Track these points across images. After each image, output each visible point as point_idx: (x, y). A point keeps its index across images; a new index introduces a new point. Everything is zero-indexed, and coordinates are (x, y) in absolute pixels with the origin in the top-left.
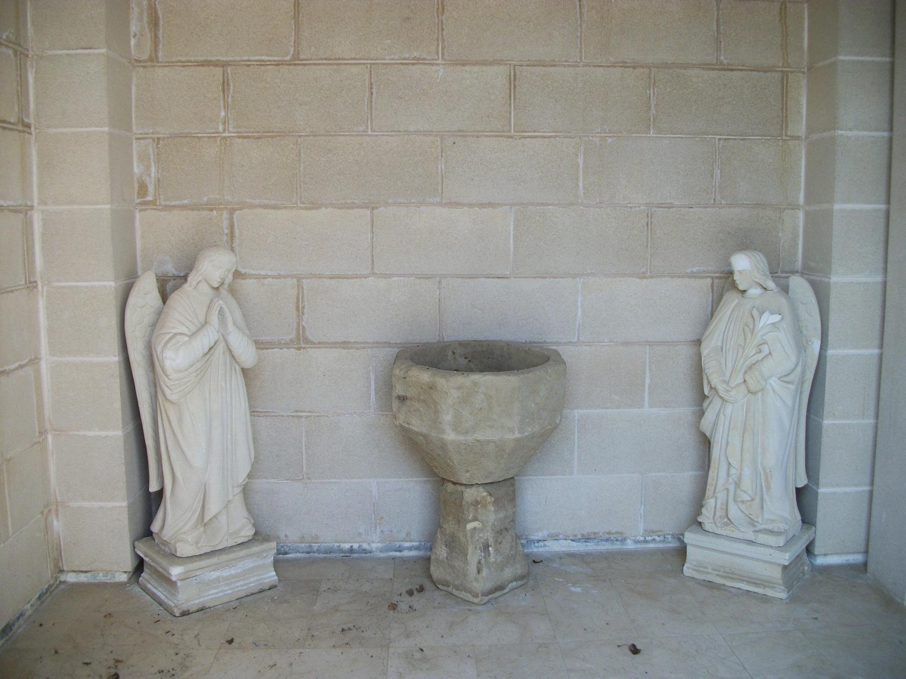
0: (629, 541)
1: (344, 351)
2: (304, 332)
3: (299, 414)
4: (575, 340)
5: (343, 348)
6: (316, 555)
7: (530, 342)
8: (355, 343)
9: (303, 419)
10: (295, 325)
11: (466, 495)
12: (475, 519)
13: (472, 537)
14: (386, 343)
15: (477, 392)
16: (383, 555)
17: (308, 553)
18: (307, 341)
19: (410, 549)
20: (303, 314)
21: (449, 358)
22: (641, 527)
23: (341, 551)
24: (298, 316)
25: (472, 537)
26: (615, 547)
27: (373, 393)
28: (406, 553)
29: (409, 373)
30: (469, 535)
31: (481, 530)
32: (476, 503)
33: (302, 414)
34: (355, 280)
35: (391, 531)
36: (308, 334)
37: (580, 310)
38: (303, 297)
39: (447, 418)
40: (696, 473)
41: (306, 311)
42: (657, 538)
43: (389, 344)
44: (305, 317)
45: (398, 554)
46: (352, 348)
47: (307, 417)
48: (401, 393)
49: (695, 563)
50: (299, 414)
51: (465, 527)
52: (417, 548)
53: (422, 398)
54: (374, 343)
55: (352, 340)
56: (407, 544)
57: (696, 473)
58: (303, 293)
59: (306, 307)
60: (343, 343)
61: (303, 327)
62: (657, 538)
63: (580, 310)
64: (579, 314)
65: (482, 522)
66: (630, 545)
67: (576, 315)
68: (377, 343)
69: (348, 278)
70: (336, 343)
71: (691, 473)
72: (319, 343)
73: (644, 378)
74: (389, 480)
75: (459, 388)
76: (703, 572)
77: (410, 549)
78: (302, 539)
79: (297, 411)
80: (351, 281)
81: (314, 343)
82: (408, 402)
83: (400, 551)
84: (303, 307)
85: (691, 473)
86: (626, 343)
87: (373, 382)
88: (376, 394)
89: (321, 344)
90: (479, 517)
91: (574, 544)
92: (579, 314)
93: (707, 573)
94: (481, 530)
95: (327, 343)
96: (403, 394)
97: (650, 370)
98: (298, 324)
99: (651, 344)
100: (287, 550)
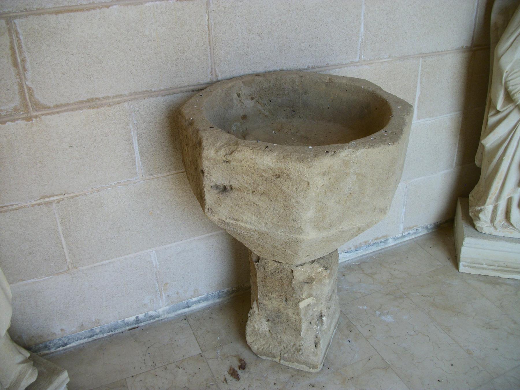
0: (390, 240)
1: (92, 112)
2: (31, 95)
3: (47, 200)
4: (357, 59)
5: (90, 107)
6: (100, 336)
7: (313, 68)
8: (104, 98)
9: (54, 205)
10: (16, 87)
11: (296, 274)
12: (310, 296)
13: (305, 314)
14: (147, 91)
15: (347, 174)
16: (172, 315)
17: (91, 336)
18: (38, 106)
19: (199, 302)
20: (25, 70)
21: (235, 103)
22: (402, 226)
23: (127, 324)
24: (18, 74)
25: (305, 314)
26: (380, 248)
27: (137, 155)
28: (194, 307)
29: (236, 155)
30: (302, 313)
31: (316, 305)
32: (310, 281)
33: (51, 199)
34: (93, 11)
35: (178, 293)
36: (38, 96)
37: (362, 25)
38: (20, 46)
39: (308, 214)
40: (447, 171)
41: (28, 65)
42: (411, 232)
43: (149, 94)
44: (29, 75)
45: (187, 310)
46: (102, 106)
47: (58, 201)
48: (221, 181)
49: (469, 260)
50: (47, 200)
51: (297, 305)
52: (206, 299)
53: (261, 188)
54: (130, 94)
55: (101, 96)
56: (194, 299)
57: (447, 171)
58: (19, 40)
59: (28, 59)
60: (89, 101)
61: (29, 89)
62: (411, 232)
63: (362, 25)
64: (362, 30)
65: (317, 297)
66: (391, 243)
67: (359, 31)
68: (135, 93)
69: (82, 10)
70: (79, 103)
71: (442, 172)
72: (57, 106)
73: (415, 92)
74: (169, 245)
75: (324, 174)
76: (479, 268)
77: (199, 302)
78: (82, 327)
79: (44, 197)
80: (86, 13)
81: (49, 108)
82: (235, 194)
83: (188, 307)
84: (23, 61)
85: (442, 172)
86: (402, 58)
87: (136, 144)
88: (142, 156)
89: (59, 108)
90: (314, 293)
91: (347, 255)
92: (362, 30)
93: (483, 269)
94: (316, 305)
95: (67, 105)
96: (227, 184)
97: (421, 83)
98: (21, 86)
99: (423, 55)
100: (66, 341)
